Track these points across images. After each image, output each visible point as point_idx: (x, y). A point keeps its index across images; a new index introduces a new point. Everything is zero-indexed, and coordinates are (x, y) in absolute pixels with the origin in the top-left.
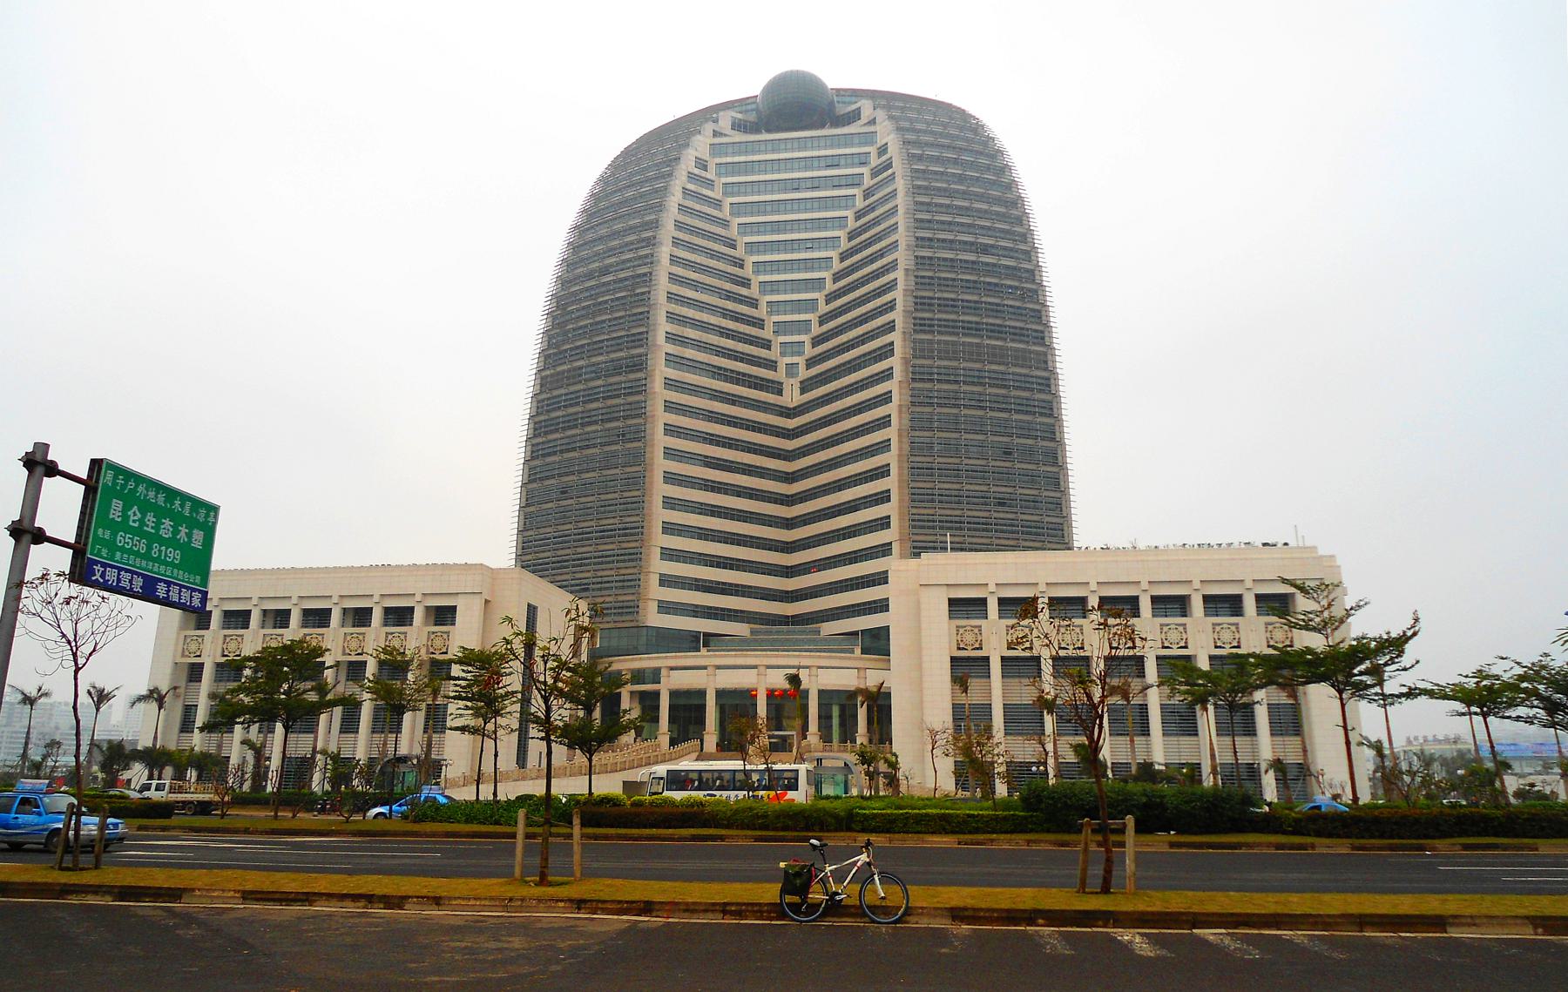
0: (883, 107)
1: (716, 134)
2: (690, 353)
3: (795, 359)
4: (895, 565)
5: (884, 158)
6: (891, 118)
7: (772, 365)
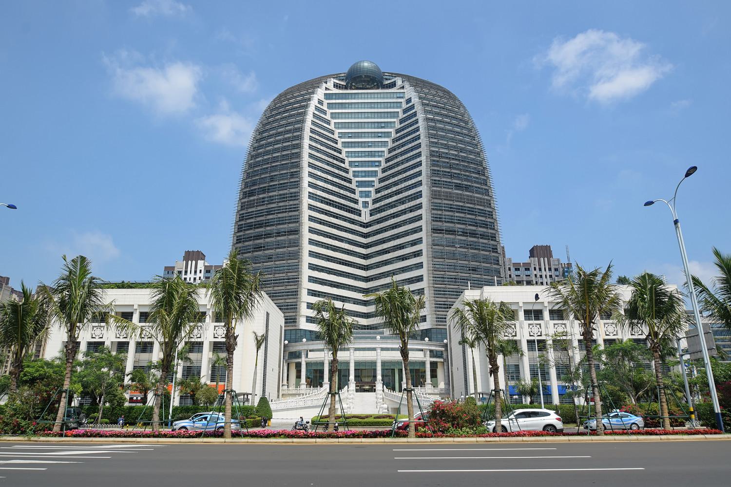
1: (326, 89)
2: (319, 193)
3: (367, 199)
5: (410, 104)
7: (356, 202)
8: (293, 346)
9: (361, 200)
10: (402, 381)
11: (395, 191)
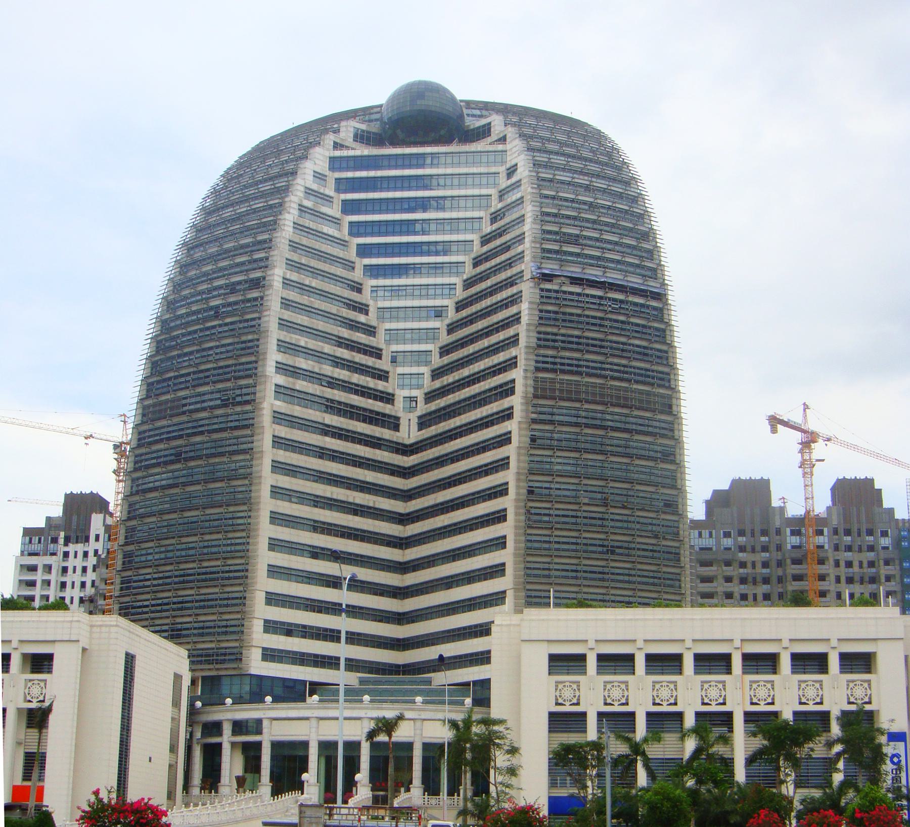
0: (514, 125)
1: (336, 146)
2: (301, 385)
3: (414, 393)
4: (501, 617)
5: (514, 179)
6: (522, 136)
7: (388, 398)
8: (208, 713)
9: (401, 394)
10: (411, 783)
11: (468, 377)
